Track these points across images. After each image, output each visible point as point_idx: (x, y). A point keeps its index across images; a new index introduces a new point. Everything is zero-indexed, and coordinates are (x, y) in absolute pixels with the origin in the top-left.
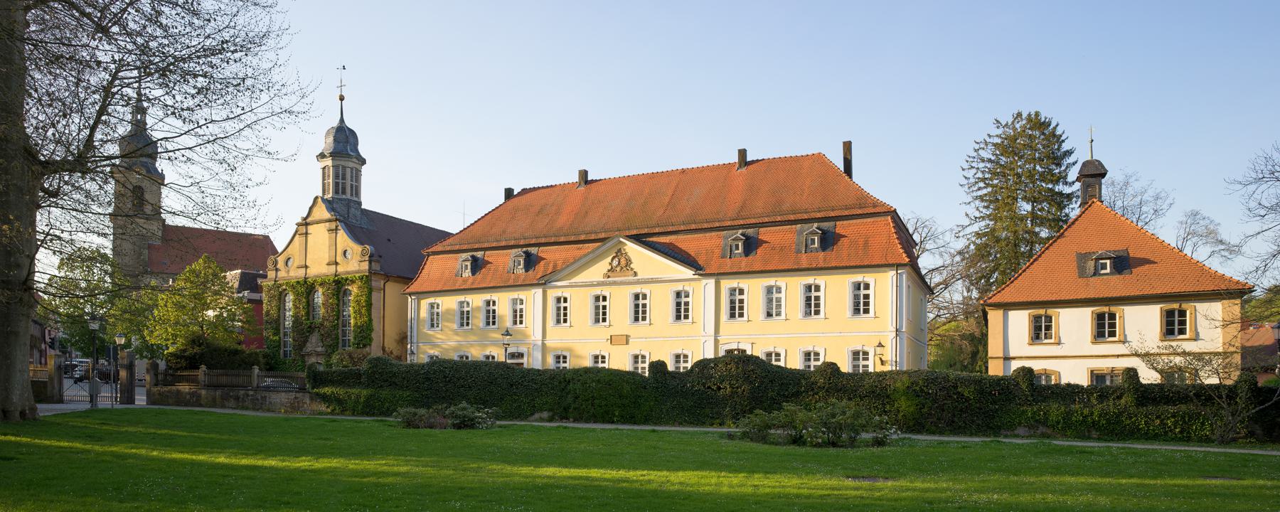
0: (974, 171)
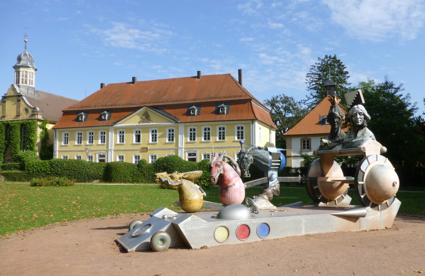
0: (309, 78)
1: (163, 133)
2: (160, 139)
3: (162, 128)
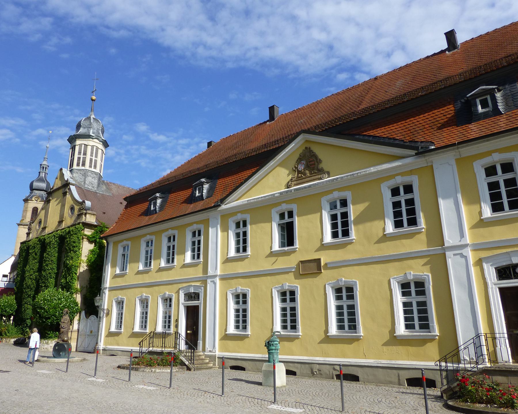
1: (366, 204)
2: (361, 227)
3: (365, 187)
